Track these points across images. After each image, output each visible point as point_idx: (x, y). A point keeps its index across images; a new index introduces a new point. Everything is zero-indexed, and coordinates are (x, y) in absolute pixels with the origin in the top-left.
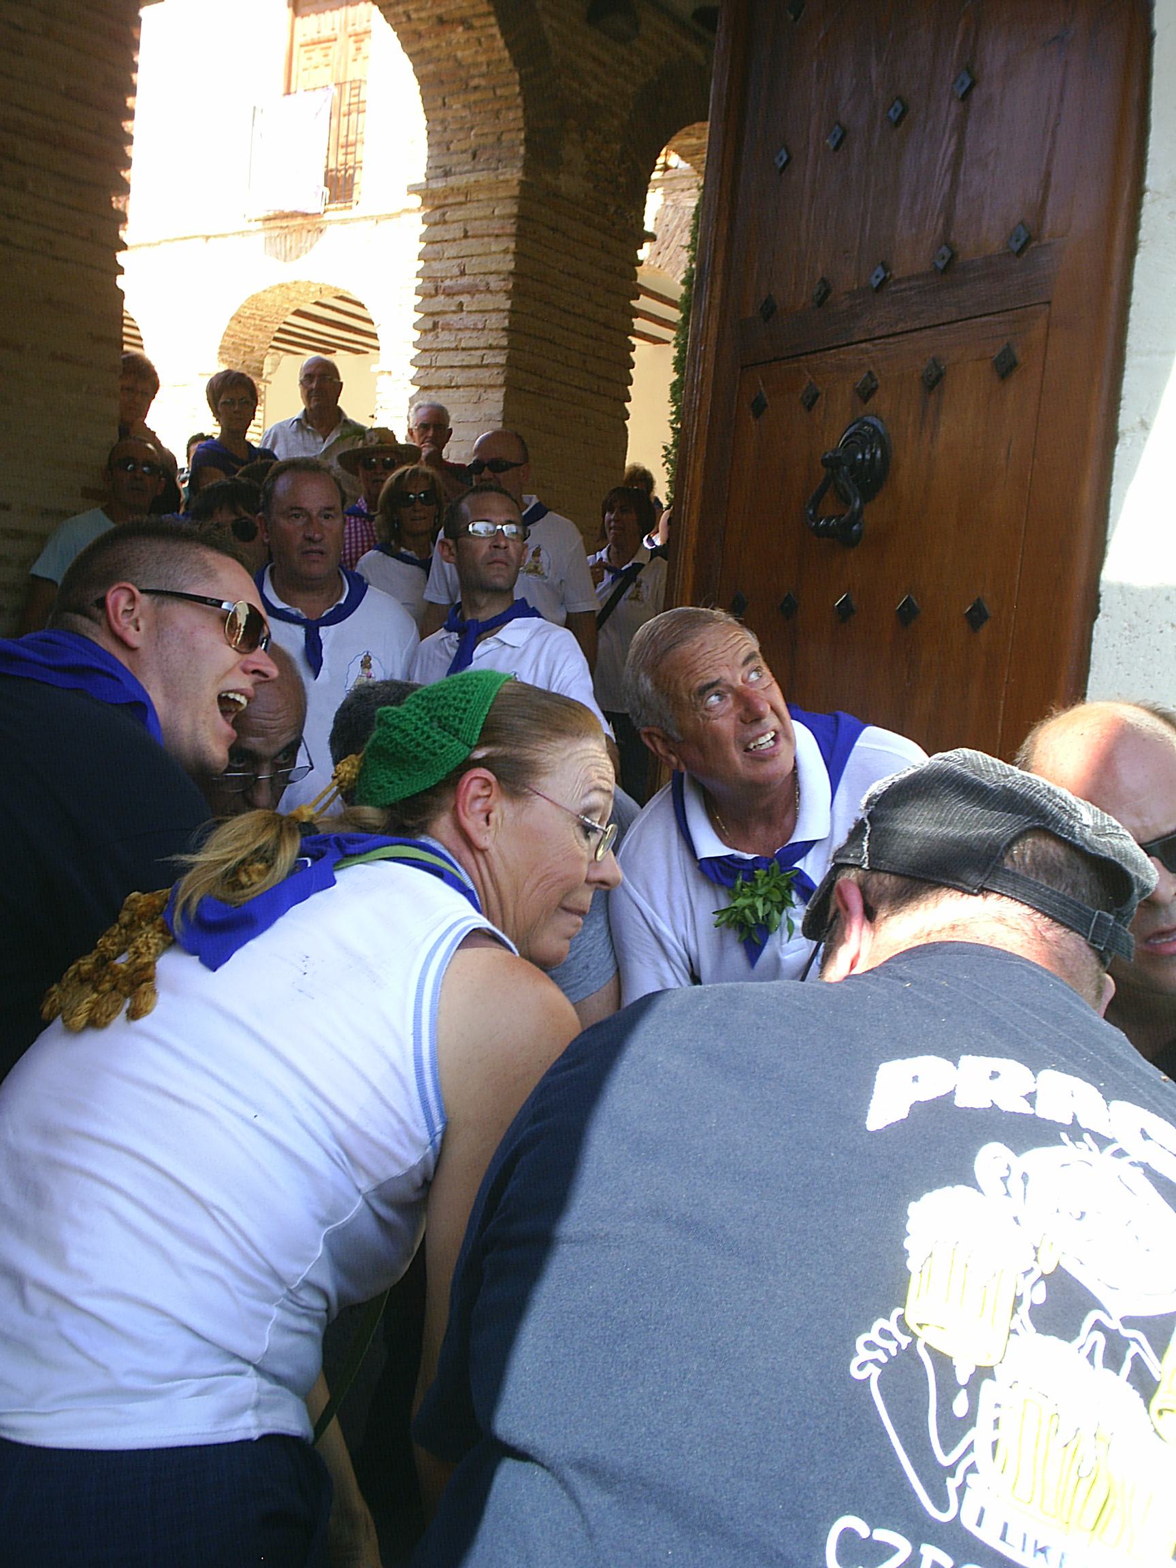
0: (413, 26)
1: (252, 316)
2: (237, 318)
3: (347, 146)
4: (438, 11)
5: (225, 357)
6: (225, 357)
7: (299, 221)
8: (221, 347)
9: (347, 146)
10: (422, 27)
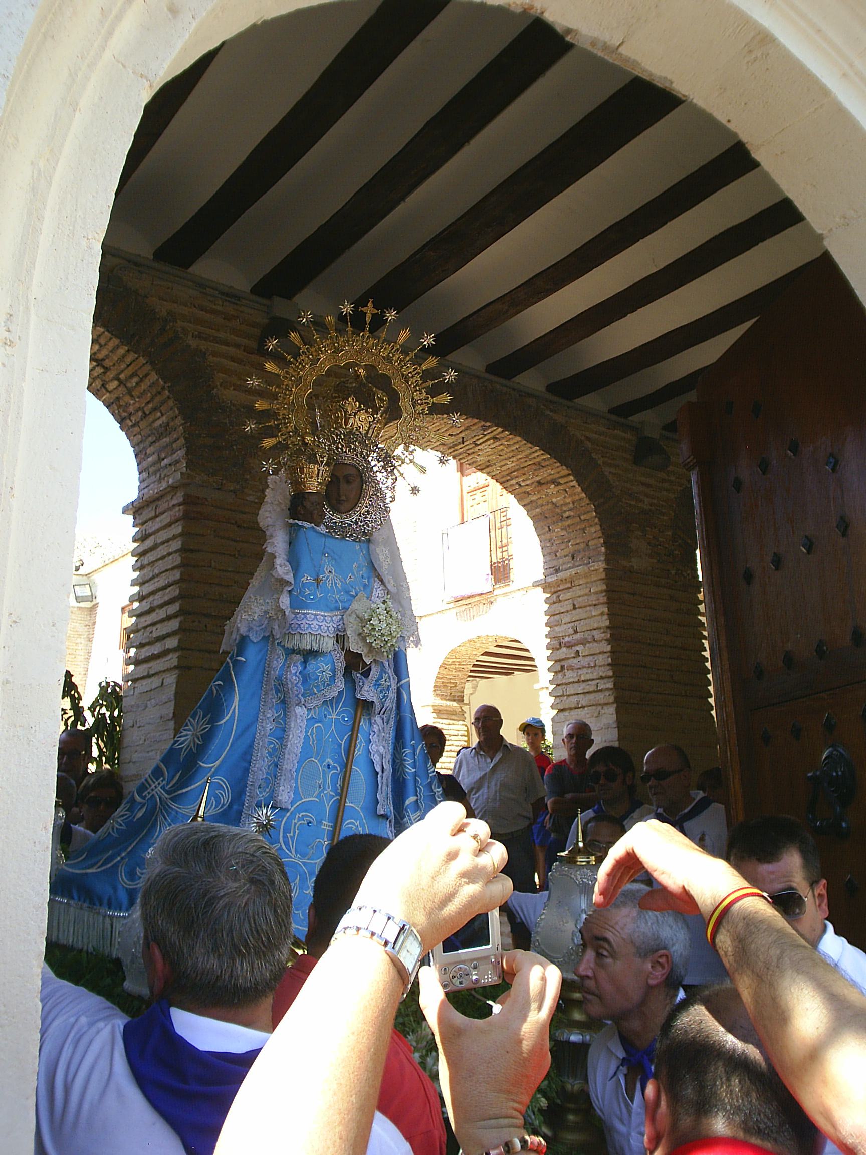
0: (523, 489)
1: (453, 663)
2: (443, 666)
3: (502, 547)
4: (538, 479)
5: (438, 692)
6: (438, 692)
7: (477, 598)
8: (435, 686)
9: (502, 547)
10: (529, 489)
